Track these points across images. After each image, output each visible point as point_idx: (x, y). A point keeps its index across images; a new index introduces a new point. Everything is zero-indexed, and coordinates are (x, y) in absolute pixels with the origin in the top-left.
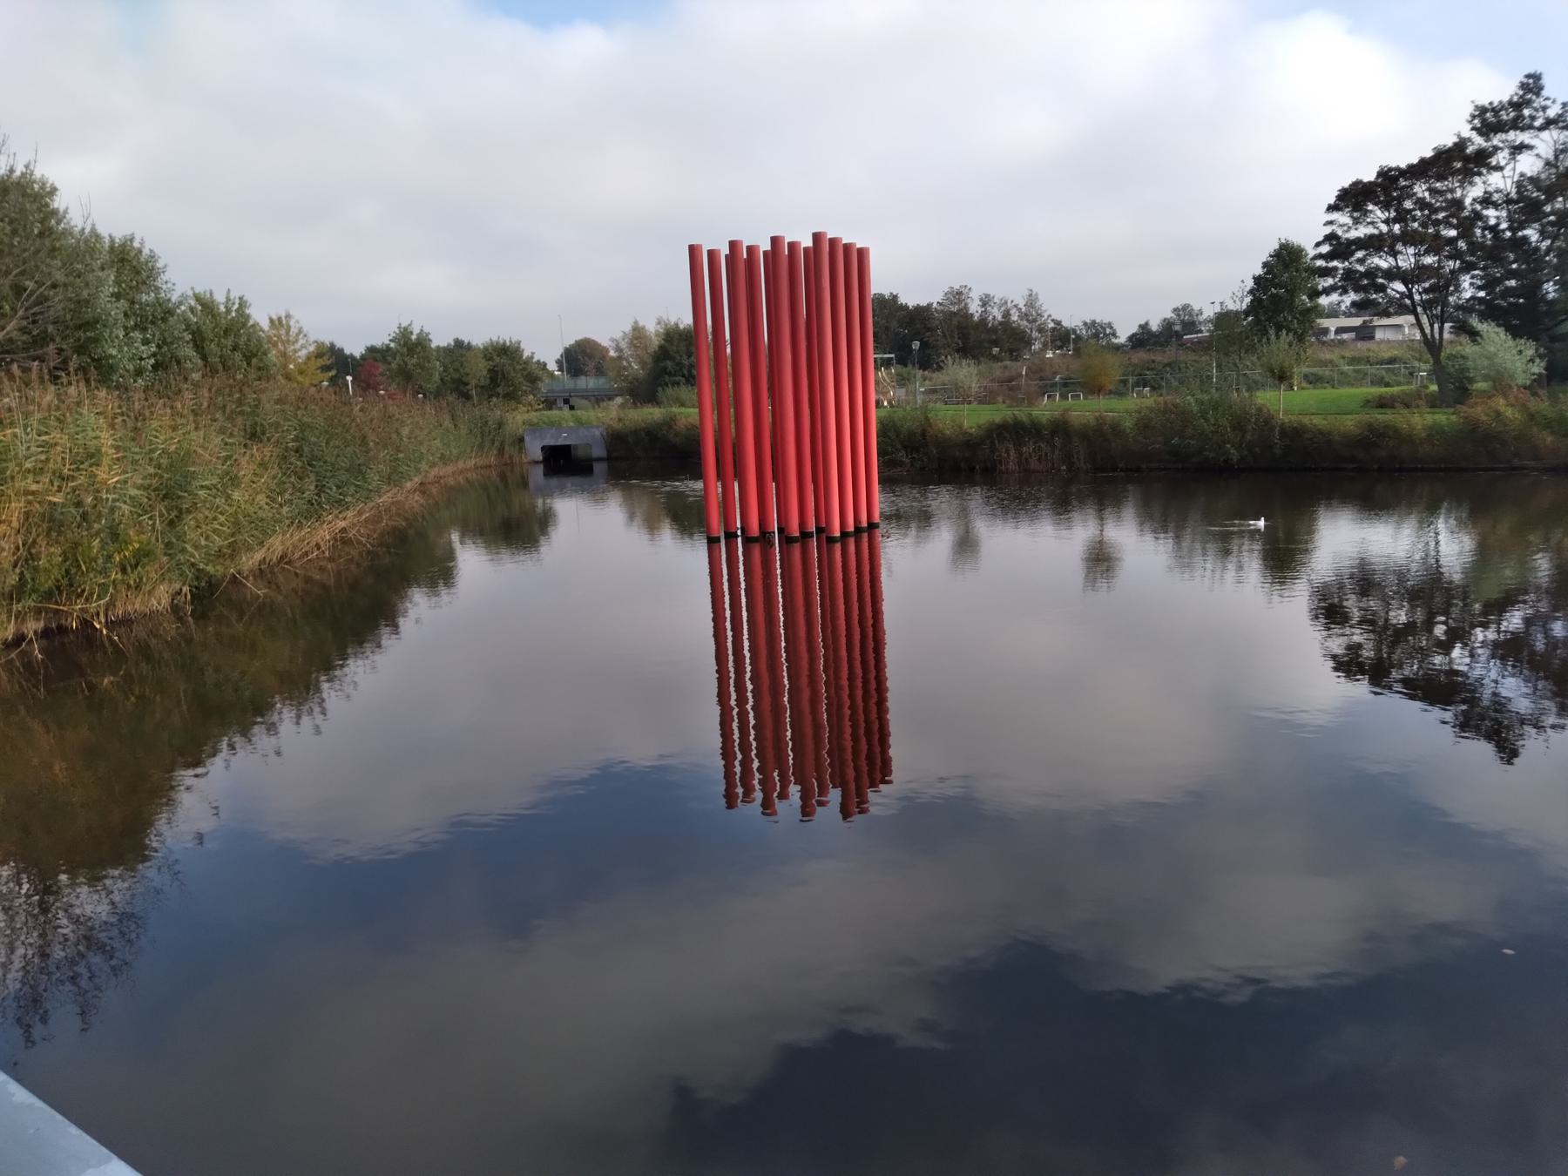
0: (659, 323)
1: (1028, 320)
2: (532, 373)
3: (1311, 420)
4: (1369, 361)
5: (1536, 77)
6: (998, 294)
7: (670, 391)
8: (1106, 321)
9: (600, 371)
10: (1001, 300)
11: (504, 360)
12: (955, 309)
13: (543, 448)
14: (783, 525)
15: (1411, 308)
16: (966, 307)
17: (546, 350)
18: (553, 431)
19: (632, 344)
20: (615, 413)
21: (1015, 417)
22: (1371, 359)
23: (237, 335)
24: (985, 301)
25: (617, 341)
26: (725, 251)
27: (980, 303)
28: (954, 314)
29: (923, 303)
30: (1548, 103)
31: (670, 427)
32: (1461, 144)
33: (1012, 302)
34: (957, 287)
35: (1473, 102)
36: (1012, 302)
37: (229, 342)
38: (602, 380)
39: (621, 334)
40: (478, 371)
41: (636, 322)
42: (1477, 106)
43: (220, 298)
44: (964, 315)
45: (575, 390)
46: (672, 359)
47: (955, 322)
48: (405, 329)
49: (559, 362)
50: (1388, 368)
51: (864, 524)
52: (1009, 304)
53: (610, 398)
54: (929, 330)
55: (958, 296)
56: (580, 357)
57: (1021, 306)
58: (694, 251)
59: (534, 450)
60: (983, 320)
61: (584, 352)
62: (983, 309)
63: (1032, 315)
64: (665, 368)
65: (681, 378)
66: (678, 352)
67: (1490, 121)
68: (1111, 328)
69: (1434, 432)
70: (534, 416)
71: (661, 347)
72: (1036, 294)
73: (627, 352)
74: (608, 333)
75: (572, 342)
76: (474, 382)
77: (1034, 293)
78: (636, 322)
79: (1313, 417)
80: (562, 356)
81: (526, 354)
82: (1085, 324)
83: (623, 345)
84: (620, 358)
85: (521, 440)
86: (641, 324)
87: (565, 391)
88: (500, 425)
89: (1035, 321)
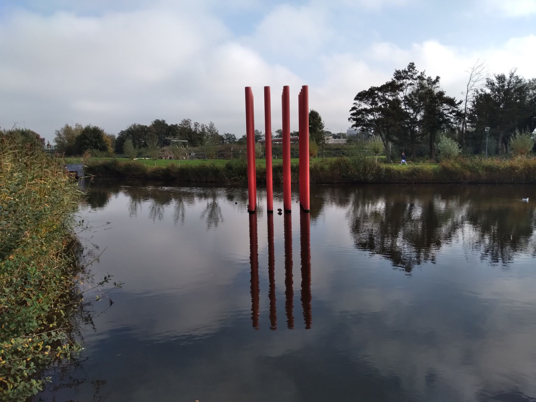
0: (77, 125)
3: (393, 167)
4: (330, 149)
5: (413, 64)
6: (201, 123)
8: (232, 134)
10: (202, 125)
14: (286, 209)
15: (264, 138)
16: (190, 126)
21: (173, 165)
22: (331, 149)
25: (58, 131)
27: (195, 125)
30: (417, 72)
32: (393, 82)
33: (206, 125)
35: (395, 69)
36: (206, 125)
39: (61, 129)
42: (396, 71)
46: (88, 139)
50: (336, 152)
52: (204, 126)
55: (187, 122)
57: (208, 126)
60: (195, 132)
62: (195, 127)
63: (212, 130)
65: (92, 146)
66: (90, 136)
67: (399, 75)
68: (234, 136)
69: (434, 170)
72: (213, 124)
77: (212, 123)
79: (393, 166)
82: (226, 134)
83: (61, 133)
86: (70, 125)
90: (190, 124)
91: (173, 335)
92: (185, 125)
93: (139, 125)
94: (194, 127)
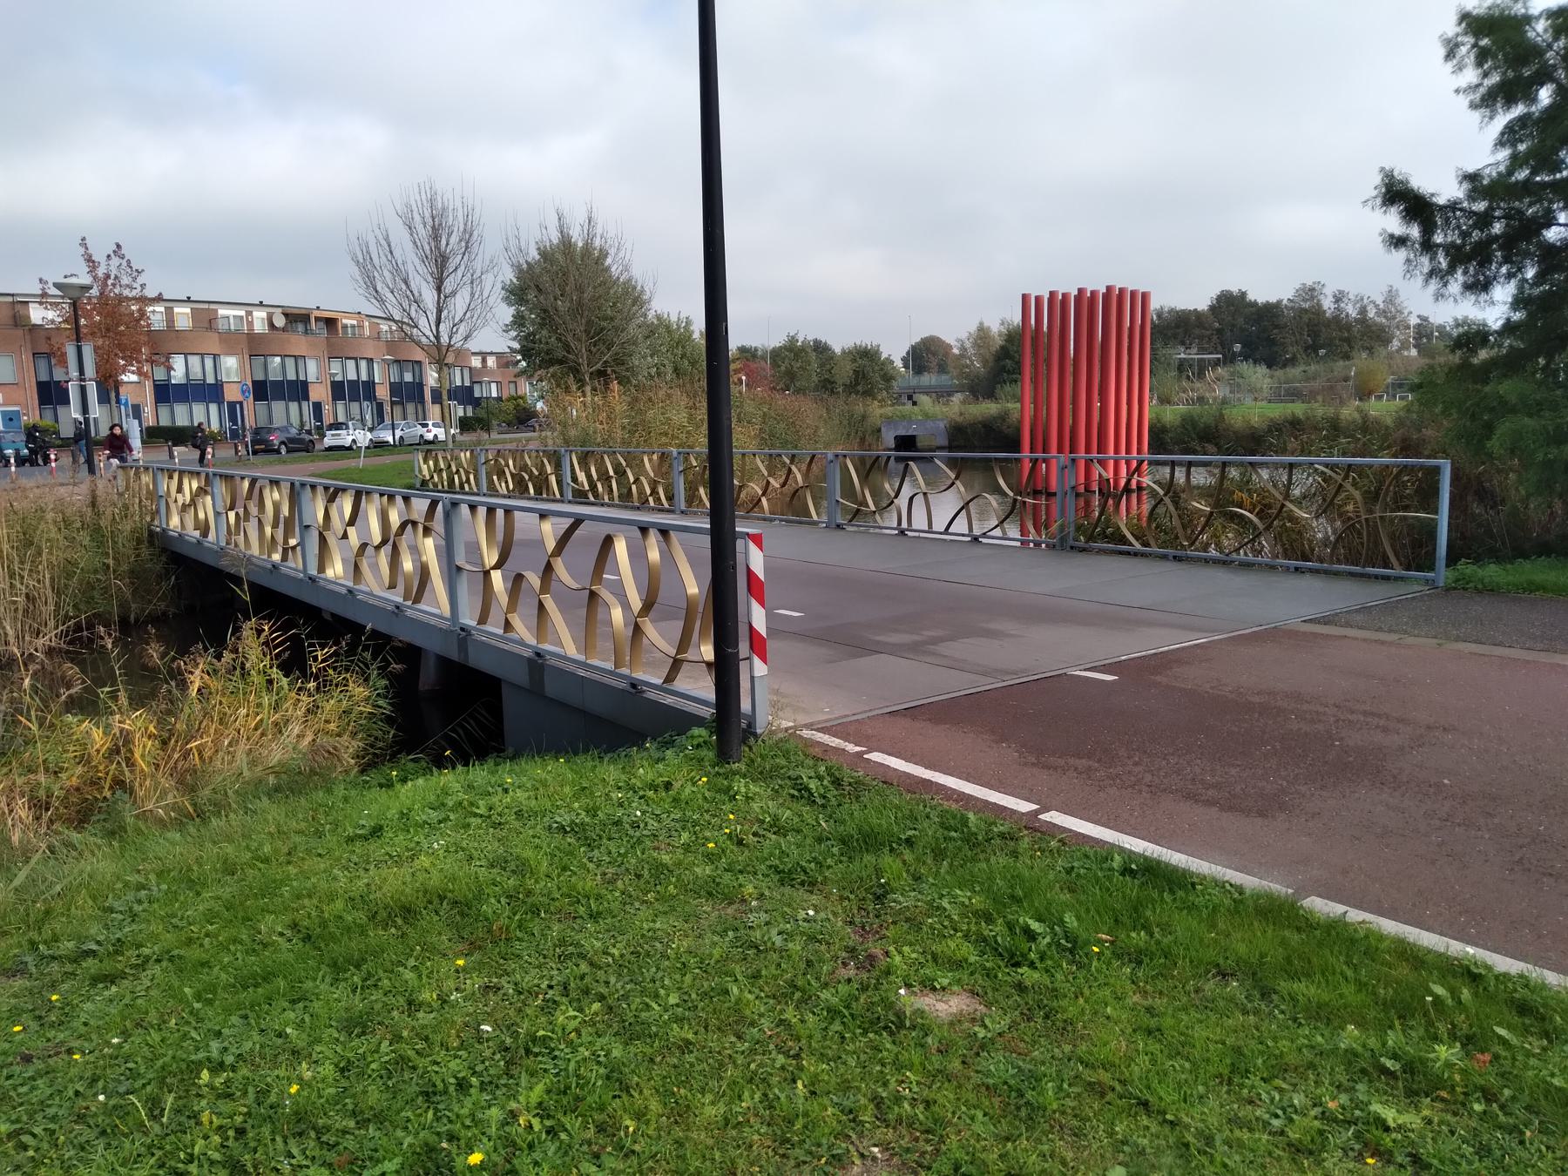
0: (1003, 324)
1: (1386, 317)
2: (885, 373)
6: (1353, 290)
7: (1008, 388)
9: (942, 369)
11: (865, 362)
12: (1306, 305)
13: (896, 437)
16: (1319, 305)
17: (895, 351)
18: (905, 423)
19: (975, 345)
20: (958, 408)
23: (683, 347)
24: (1338, 298)
26: (1046, 296)
28: (1306, 311)
29: (1273, 300)
31: (1004, 420)
34: (1309, 283)
37: (679, 352)
38: (944, 377)
40: (844, 373)
41: (981, 324)
43: (674, 318)
44: (1318, 311)
45: (919, 387)
47: (1305, 318)
48: (793, 337)
49: (905, 360)
51: (1134, 496)
52: (1365, 301)
53: (950, 394)
54: (1277, 327)
55: (1310, 292)
56: (925, 355)
57: (1379, 301)
58: (1025, 298)
59: (889, 438)
61: (928, 350)
64: (1004, 367)
70: (889, 410)
71: (1002, 347)
73: (971, 351)
74: (955, 332)
75: (918, 340)
76: (840, 382)
78: (981, 324)
80: (908, 353)
81: (884, 356)
83: (968, 345)
84: (962, 356)
85: (879, 430)
86: (986, 324)
87: (909, 388)
88: (864, 417)
89: (1394, 318)
90: (1322, 297)
91: (1539, 577)
92: (1305, 300)
93: (1171, 311)
94: (1333, 306)
